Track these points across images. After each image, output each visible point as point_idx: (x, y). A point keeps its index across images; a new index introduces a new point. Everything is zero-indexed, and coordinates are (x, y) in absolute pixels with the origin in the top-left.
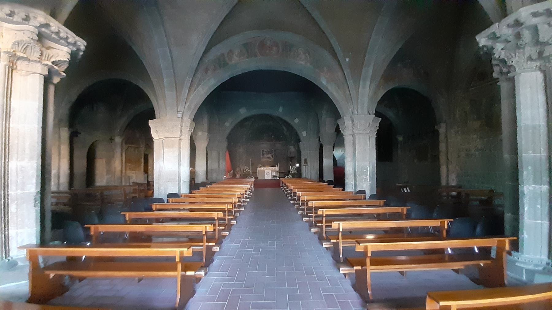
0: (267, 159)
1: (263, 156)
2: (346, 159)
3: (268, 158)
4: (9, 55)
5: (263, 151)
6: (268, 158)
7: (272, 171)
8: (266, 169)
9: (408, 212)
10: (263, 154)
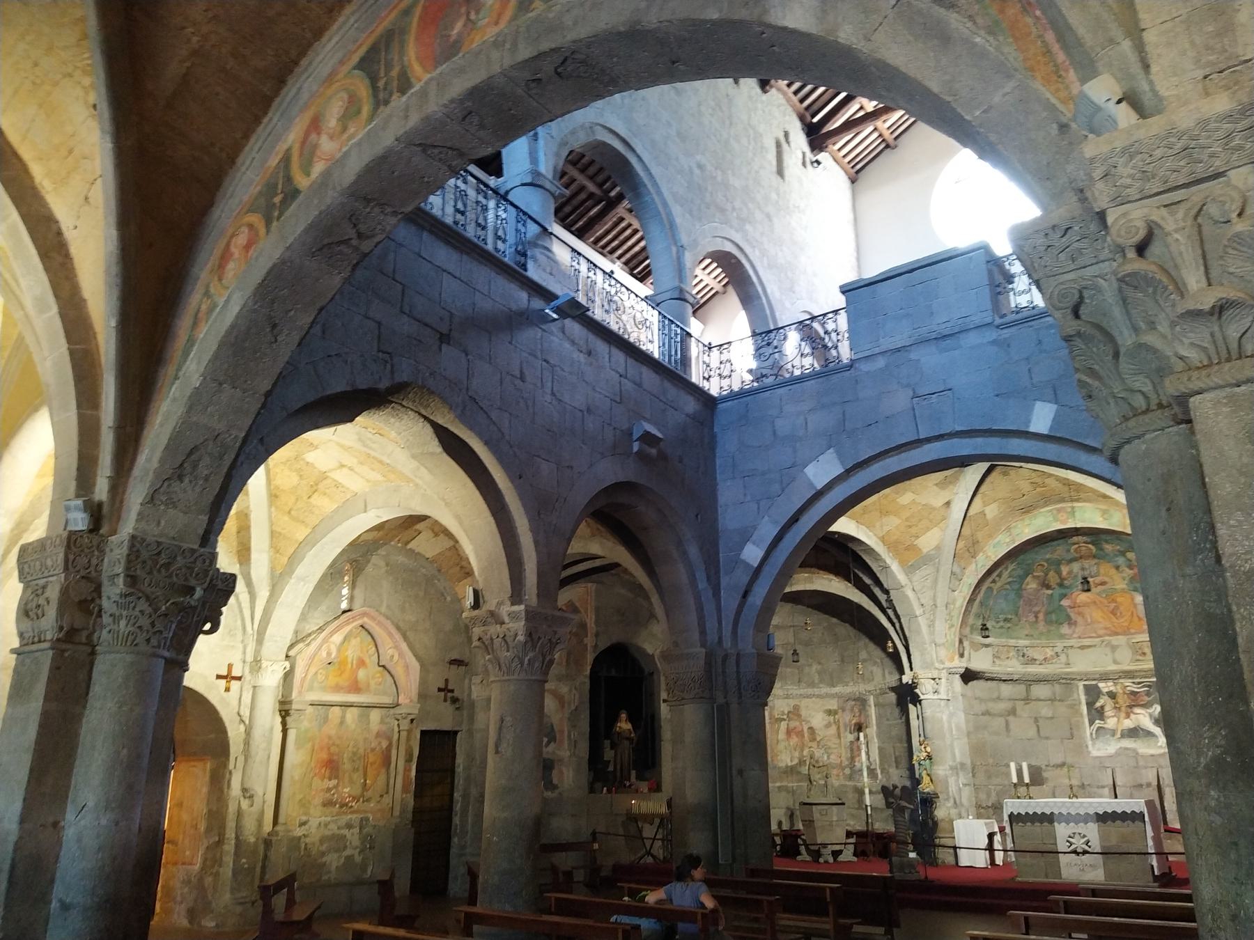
1: (1098, 723)
3: (1134, 733)
10: (1097, 714)
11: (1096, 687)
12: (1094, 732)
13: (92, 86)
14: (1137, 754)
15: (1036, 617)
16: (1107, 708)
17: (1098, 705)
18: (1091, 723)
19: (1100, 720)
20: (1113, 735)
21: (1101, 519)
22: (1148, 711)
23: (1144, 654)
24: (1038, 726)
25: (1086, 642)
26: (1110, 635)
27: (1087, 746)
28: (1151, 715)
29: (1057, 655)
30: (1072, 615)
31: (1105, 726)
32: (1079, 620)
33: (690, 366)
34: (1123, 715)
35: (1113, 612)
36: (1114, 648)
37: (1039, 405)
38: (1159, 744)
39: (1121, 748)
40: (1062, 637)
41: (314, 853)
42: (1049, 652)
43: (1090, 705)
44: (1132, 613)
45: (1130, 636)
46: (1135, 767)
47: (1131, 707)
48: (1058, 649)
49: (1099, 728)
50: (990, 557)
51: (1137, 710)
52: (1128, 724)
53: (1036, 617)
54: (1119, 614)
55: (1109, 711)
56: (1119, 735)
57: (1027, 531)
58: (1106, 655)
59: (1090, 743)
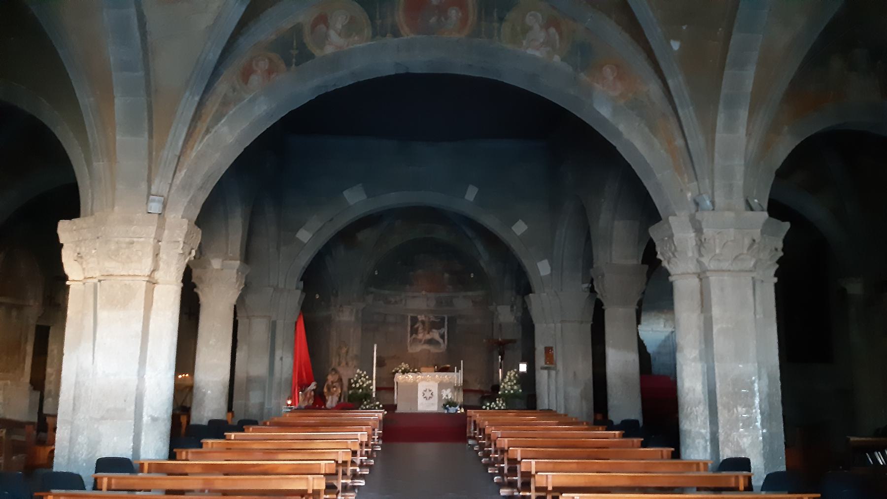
0: (426, 347)
1: (414, 336)
3: (431, 342)
5: (414, 320)
6: (431, 342)
8: (422, 380)
10: (414, 331)
13: (687, 394)
16: (420, 328)
17: (416, 326)
28: (439, 334)
29: (401, 300)
33: (714, 494)
34: (426, 332)
37: (519, 234)
43: (412, 327)
49: (414, 339)
51: (434, 330)
52: (428, 337)
56: (423, 342)
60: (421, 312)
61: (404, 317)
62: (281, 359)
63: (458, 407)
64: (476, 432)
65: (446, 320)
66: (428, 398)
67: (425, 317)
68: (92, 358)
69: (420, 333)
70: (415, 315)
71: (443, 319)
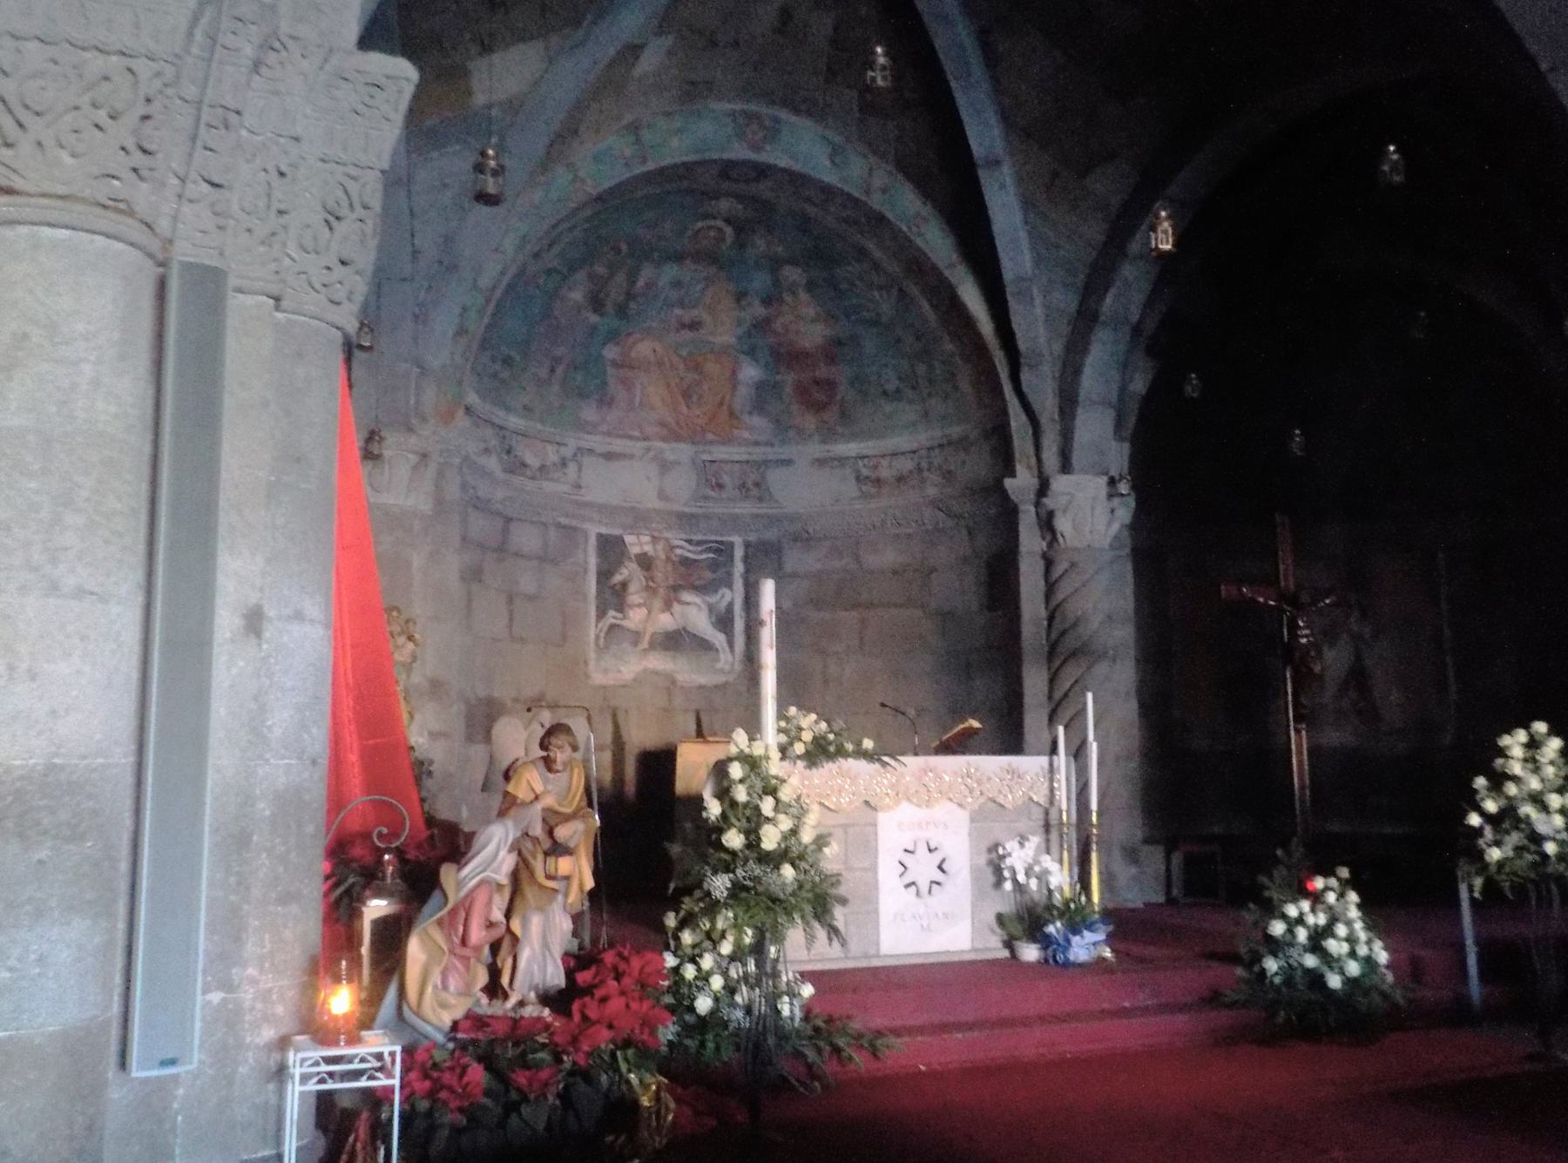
0: (659, 662)
1: (612, 616)
2: (946, 617)
3: (674, 641)
4: (1532, 881)
5: (611, 549)
6: (674, 641)
7: (987, 813)
8: (901, 794)
9: (708, 1018)
10: (613, 596)
11: (620, 541)
12: (602, 635)
14: (674, 682)
15: (553, 370)
16: (632, 588)
17: (618, 578)
18: (601, 614)
19: (616, 610)
20: (635, 643)
21: (828, 163)
22: (708, 599)
23: (720, 486)
24: (511, 613)
25: (618, 445)
26: (664, 439)
27: (586, 663)
28: (711, 608)
29: (564, 463)
30: (611, 381)
31: (625, 623)
32: (620, 394)
34: (658, 603)
35: (686, 395)
36: (665, 467)
38: (720, 665)
39: (645, 670)
40: (582, 427)
41: (923, 437)
42: (552, 456)
43: (604, 575)
44: (723, 398)
45: (701, 448)
46: (665, 710)
47: (675, 588)
48: (567, 452)
49: (612, 627)
50: (583, 181)
51: (687, 596)
52: (665, 621)
53: (553, 370)
54: (695, 398)
55: (635, 596)
56: (645, 644)
57: (675, 142)
58: (648, 478)
59: (592, 655)
60: (639, 519)
61: (570, 534)
62: (254, 621)
63: (618, 946)
64: (216, 997)
65: (739, 553)
66: (924, 889)
67: (655, 539)
68: (60, 192)
69: (631, 607)
70: (617, 532)
71: (724, 550)
